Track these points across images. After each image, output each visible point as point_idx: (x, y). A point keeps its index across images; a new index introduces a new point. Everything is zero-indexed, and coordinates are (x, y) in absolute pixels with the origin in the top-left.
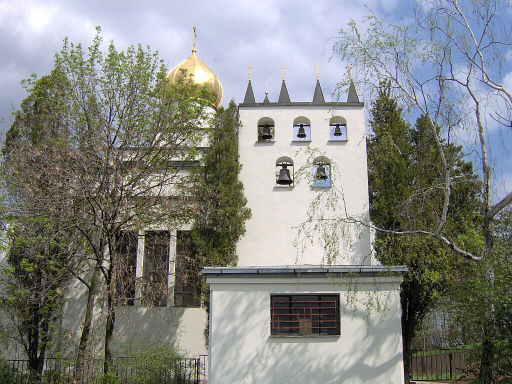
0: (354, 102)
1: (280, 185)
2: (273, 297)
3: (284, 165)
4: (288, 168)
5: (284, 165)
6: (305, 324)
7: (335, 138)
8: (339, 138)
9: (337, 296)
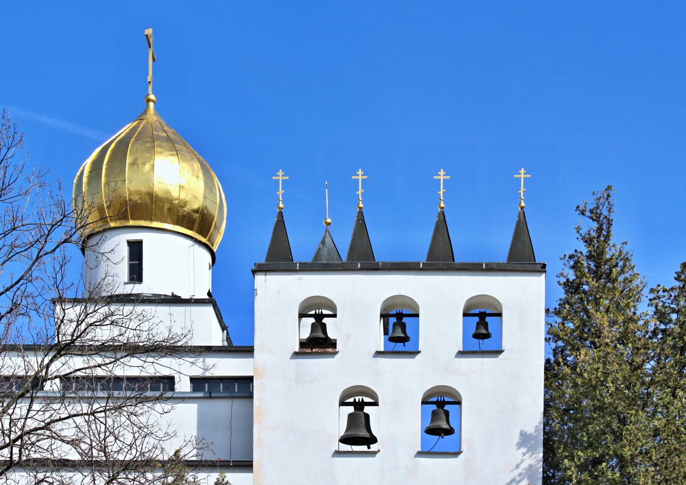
7: (475, 344)
8: (486, 344)
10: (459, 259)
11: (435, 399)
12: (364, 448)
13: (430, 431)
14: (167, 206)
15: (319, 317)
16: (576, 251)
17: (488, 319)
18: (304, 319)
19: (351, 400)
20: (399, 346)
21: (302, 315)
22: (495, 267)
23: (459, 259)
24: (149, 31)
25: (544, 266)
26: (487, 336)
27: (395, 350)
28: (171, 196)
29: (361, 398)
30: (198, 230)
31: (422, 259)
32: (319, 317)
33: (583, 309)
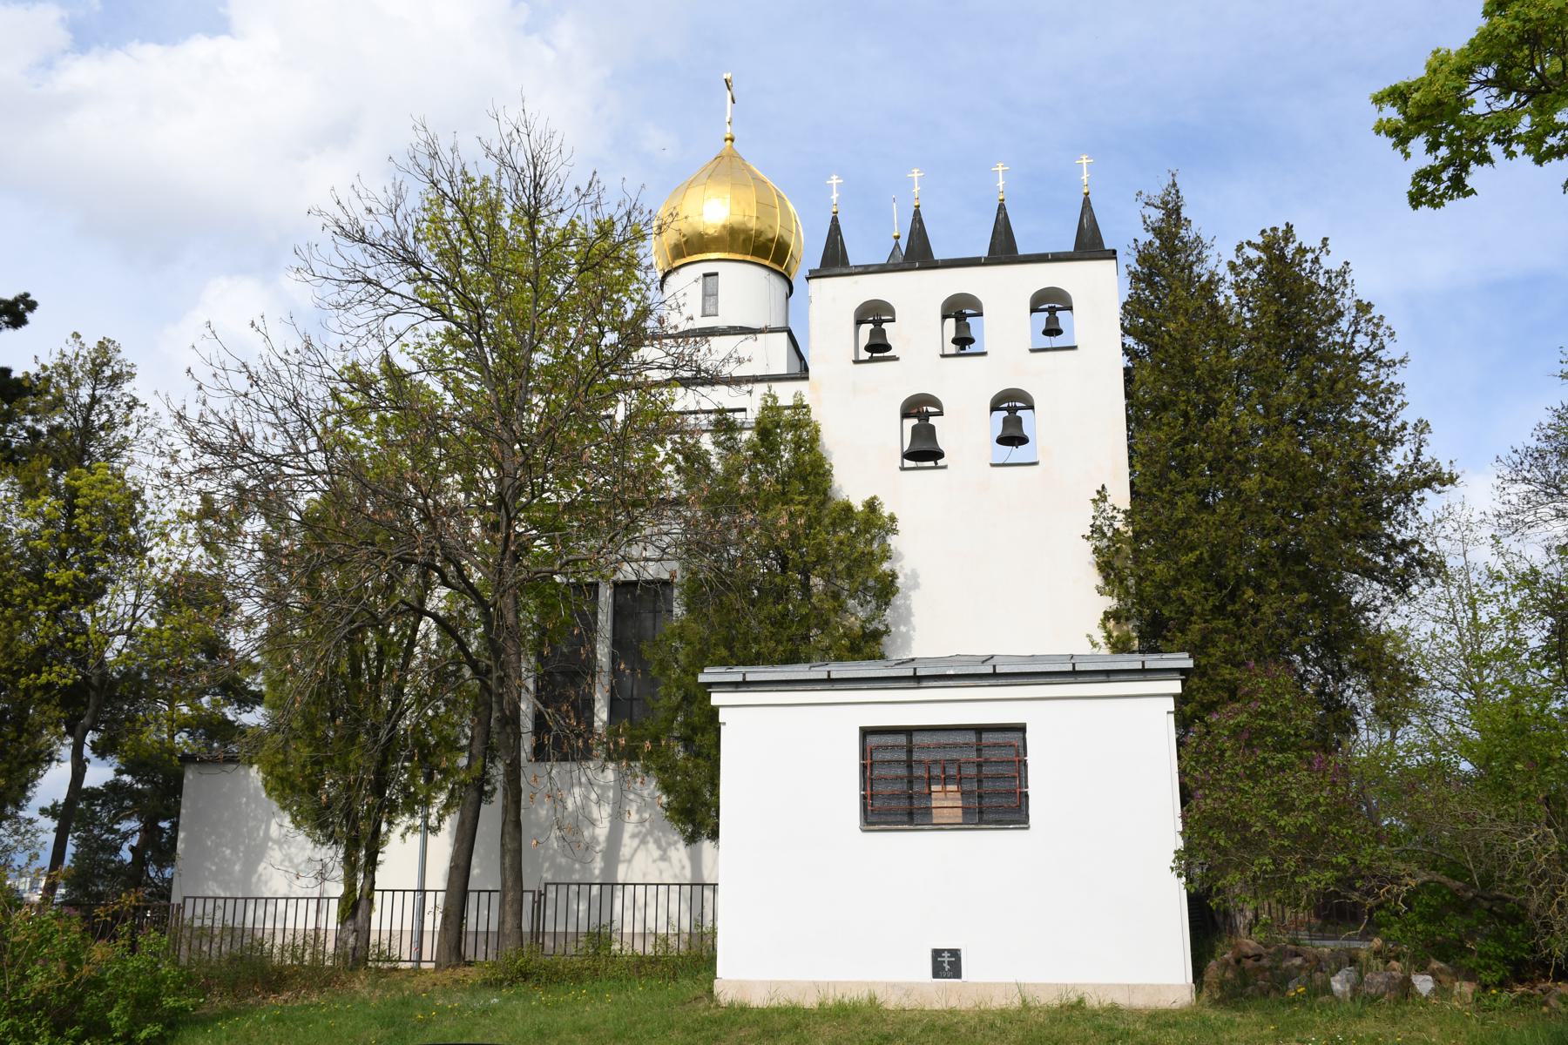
0: (1089, 245)
2: (866, 732)
3: (919, 409)
4: (932, 420)
5: (919, 409)
6: (946, 800)
9: (1021, 729)
12: (931, 464)
14: (742, 237)
17: (1058, 314)
25: (1114, 252)
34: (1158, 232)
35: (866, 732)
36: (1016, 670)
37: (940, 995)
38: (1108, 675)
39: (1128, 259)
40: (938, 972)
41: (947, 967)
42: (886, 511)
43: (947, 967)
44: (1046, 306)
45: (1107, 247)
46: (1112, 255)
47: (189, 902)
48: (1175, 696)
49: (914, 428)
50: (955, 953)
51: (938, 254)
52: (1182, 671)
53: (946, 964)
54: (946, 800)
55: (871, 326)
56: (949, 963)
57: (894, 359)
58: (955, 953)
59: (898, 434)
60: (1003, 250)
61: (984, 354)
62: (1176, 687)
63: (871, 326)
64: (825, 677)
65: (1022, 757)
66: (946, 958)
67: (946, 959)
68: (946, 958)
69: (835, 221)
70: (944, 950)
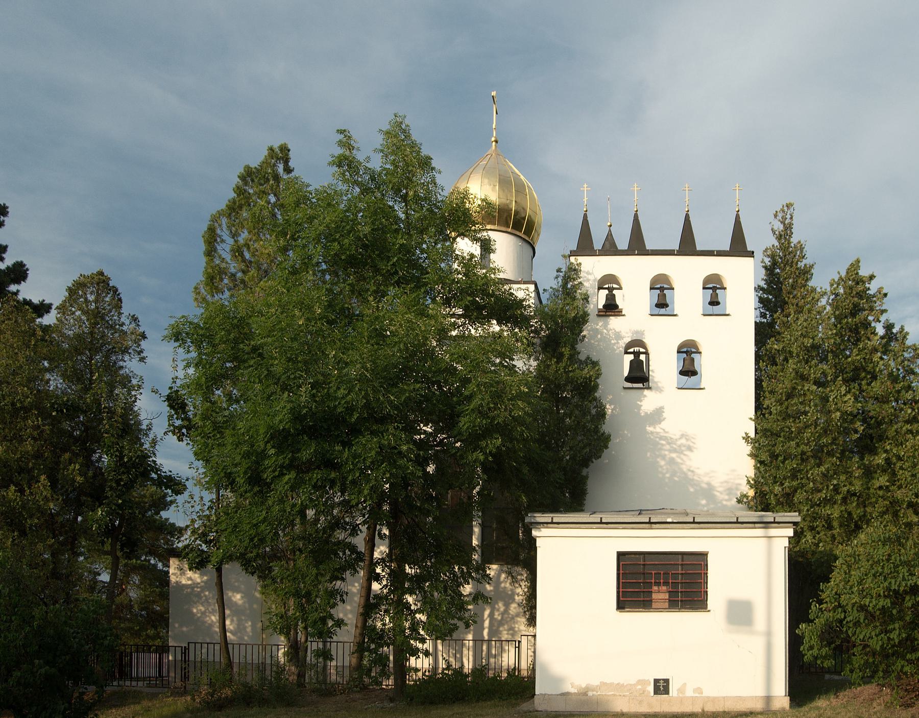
1: (629, 385)
2: (621, 555)
6: (660, 595)
7: (657, 311)
8: (716, 309)
9: (700, 559)
10: (699, 247)
11: (685, 350)
12: (640, 385)
13: (683, 373)
15: (610, 290)
16: (173, 379)
17: (718, 291)
18: (601, 290)
19: (632, 350)
20: (663, 311)
21: (600, 288)
22: (722, 253)
23: (699, 247)
24: (494, 93)
25: (753, 252)
26: (718, 303)
27: (660, 313)
28: (488, 178)
29: (638, 348)
30: (803, 553)
31: (676, 247)
32: (610, 290)
33: (12, 295)
34: (779, 238)
35: (621, 555)
36: (728, 521)
37: (660, 704)
38: (738, 523)
39: (759, 255)
40: (657, 691)
41: (662, 689)
42: (665, 415)
43: (662, 689)
44: (658, 286)
45: (749, 249)
46: (751, 254)
47: (192, 646)
48: (789, 538)
49: (631, 362)
50: (667, 681)
51: (649, 246)
52: (795, 524)
53: (661, 687)
54: (660, 595)
55: (606, 292)
56: (663, 686)
57: (624, 315)
58: (667, 681)
59: (704, 363)
60: (637, 246)
61: (728, 315)
62: (790, 532)
63: (606, 292)
64: (648, 521)
65: (706, 572)
66: (661, 684)
67: (662, 684)
68: (661, 684)
69: (585, 216)
70: (660, 680)
